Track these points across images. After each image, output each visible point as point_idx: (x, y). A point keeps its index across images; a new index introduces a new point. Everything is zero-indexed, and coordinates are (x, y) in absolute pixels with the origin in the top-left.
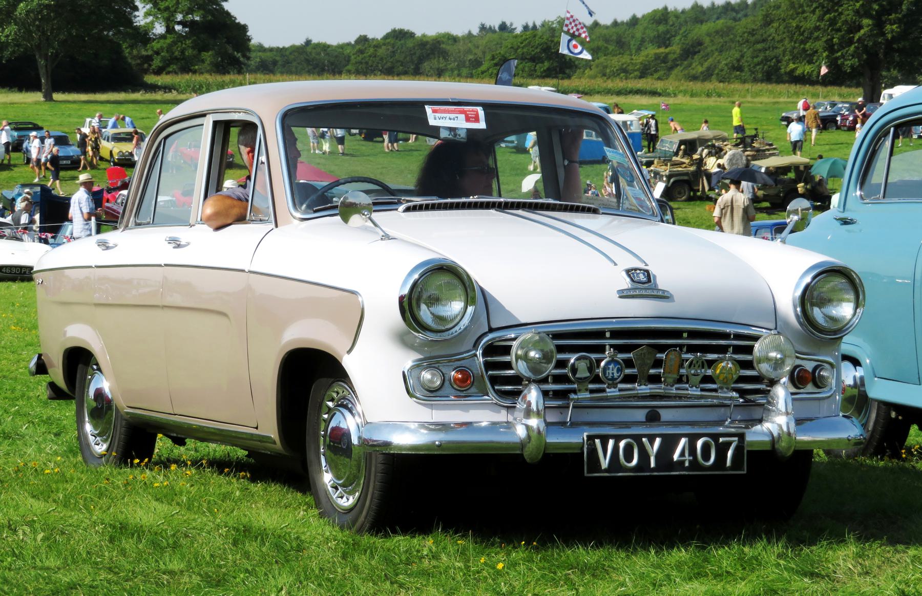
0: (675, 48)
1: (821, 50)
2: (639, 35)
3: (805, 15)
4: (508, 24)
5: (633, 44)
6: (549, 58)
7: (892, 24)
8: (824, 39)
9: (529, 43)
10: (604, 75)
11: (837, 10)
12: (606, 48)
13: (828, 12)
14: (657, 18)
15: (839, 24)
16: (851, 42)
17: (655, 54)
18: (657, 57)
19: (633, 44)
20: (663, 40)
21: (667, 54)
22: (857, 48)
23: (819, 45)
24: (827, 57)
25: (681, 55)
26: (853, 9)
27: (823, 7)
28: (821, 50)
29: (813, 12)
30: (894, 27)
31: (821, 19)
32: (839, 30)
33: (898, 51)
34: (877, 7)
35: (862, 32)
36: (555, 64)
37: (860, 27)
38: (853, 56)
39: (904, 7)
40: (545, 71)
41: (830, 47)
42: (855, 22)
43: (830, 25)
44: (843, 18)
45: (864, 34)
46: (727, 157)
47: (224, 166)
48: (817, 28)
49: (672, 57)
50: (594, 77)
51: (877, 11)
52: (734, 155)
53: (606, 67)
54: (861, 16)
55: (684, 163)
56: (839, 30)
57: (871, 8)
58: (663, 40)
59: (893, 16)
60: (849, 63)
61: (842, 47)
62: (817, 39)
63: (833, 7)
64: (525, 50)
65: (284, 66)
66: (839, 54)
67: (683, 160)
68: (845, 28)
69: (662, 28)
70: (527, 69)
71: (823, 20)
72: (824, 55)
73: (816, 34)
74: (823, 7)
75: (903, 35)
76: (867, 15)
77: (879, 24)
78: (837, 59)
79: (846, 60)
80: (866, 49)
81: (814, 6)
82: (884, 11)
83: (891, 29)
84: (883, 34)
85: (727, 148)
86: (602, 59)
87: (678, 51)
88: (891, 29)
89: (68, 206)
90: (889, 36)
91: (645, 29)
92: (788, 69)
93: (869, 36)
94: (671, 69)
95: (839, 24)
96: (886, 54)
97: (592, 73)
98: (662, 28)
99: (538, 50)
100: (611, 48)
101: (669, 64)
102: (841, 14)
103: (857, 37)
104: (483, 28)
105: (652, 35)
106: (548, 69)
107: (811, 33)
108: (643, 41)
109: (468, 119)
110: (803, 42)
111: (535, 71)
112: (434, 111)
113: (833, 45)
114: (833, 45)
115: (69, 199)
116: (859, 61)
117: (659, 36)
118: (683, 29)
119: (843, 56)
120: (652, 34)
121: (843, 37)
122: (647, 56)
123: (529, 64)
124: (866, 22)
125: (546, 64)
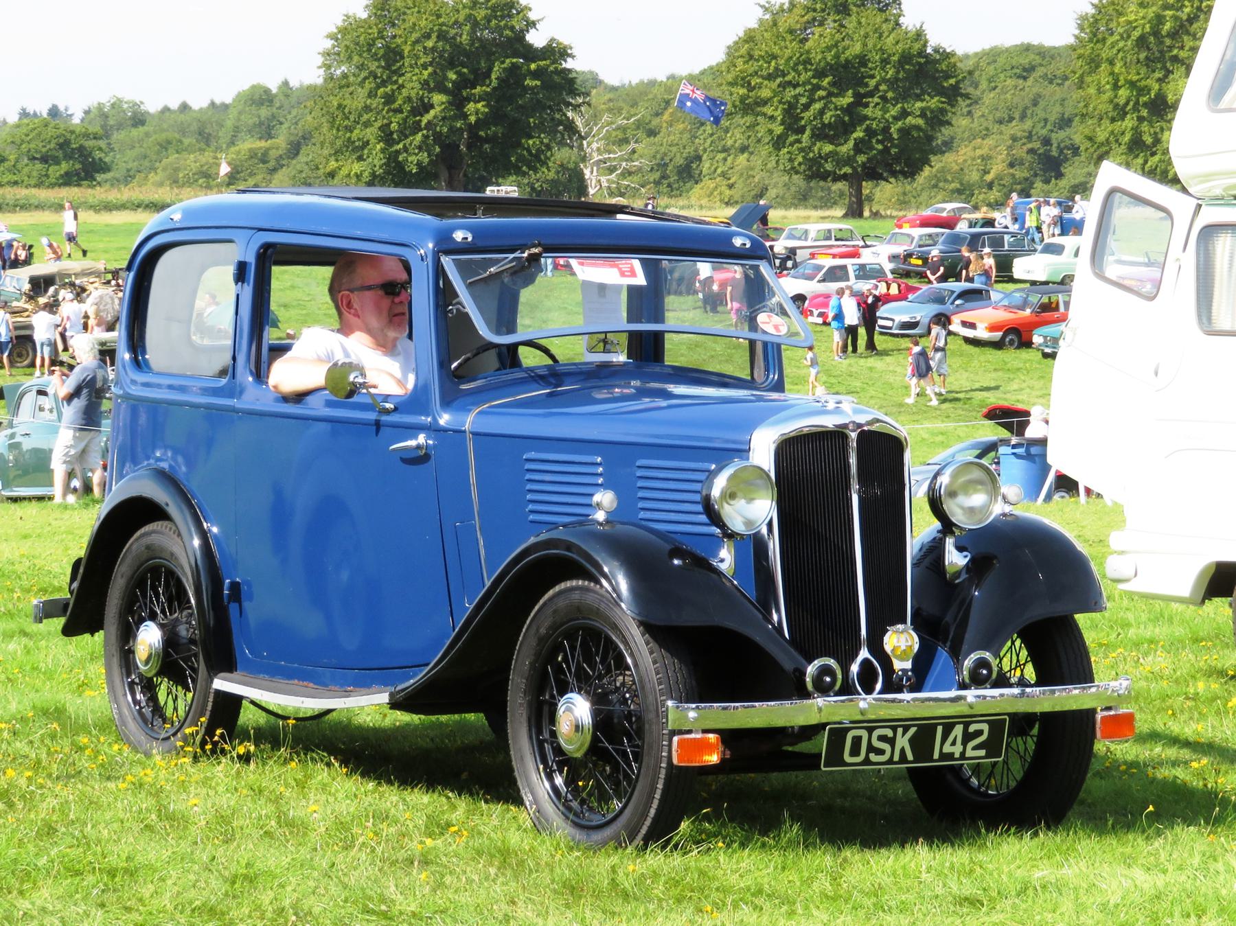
0: (281, 141)
1: (373, 141)
2: (229, 123)
3: (351, 89)
4: (62, 108)
5: (224, 135)
6: (68, 157)
7: (476, 102)
8: (378, 124)
9: (39, 134)
10: (176, 182)
11: (396, 82)
12: (180, 141)
13: (384, 83)
14: (256, 97)
15: (400, 102)
16: (417, 128)
17: (250, 150)
18: (253, 154)
19: (224, 135)
20: (266, 130)
21: (267, 150)
22: (426, 137)
23: (371, 133)
24: (383, 151)
25: (289, 151)
26: (419, 80)
27: (375, 77)
28: (373, 141)
29: (362, 84)
30: (479, 105)
31: (372, 94)
32: (399, 111)
33: (487, 140)
34: (454, 77)
35: (432, 112)
36: (78, 166)
37: (428, 107)
38: (420, 148)
39: (493, 76)
40: (62, 176)
41: (387, 137)
42: (422, 99)
43: (385, 104)
44: (405, 92)
45: (435, 117)
46: (90, 301)
47: (230, 370)
48: (367, 109)
49: (273, 154)
50: (161, 184)
51: (454, 82)
52: (101, 297)
53: (176, 170)
54: (431, 91)
55: (27, 310)
56: (399, 111)
57: (445, 78)
58: (266, 130)
59: (478, 90)
60: (414, 160)
61: (403, 135)
62: (367, 124)
63: (389, 78)
64: (32, 146)
65: (1061, 217)
66: (401, 146)
67: (27, 306)
68: (407, 107)
69: (264, 112)
70: (35, 174)
71: (376, 95)
72: (378, 147)
73: (366, 117)
74: (375, 77)
75: (495, 116)
76: (441, 88)
77: (458, 102)
78: (398, 152)
79: (410, 154)
80: (438, 137)
81: (362, 76)
82: (465, 83)
83: (476, 109)
84: (465, 116)
85: (90, 288)
86: (173, 157)
87: (284, 145)
88: (476, 109)
89: (50, 459)
90: (473, 119)
91: (240, 113)
92: (328, 170)
93: (444, 118)
94: (274, 170)
95: (400, 102)
96: (469, 147)
97: (157, 178)
98: (264, 112)
99: (52, 146)
100: (186, 141)
101: (272, 164)
102: (403, 86)
103: (425, 121)
104: (24, 114)
105: (250, 122)
106: (67, 174)
107: (360, 116)
108: (237, 129)
109: (623, 274)
110: (350, 129)
111: (47, 176)
112: (582, 264)
113: (392, 133)
114: (392, 133)
115: (51, 451)
116: (429, 155)
117: (261, 124)
118: (294, 112)
119: (406, 149)
120: (252, 121)
121: (405, 120)
122: (239, 152)
123: (39, 166)
124: (438, 98)
125: (64, 167)
